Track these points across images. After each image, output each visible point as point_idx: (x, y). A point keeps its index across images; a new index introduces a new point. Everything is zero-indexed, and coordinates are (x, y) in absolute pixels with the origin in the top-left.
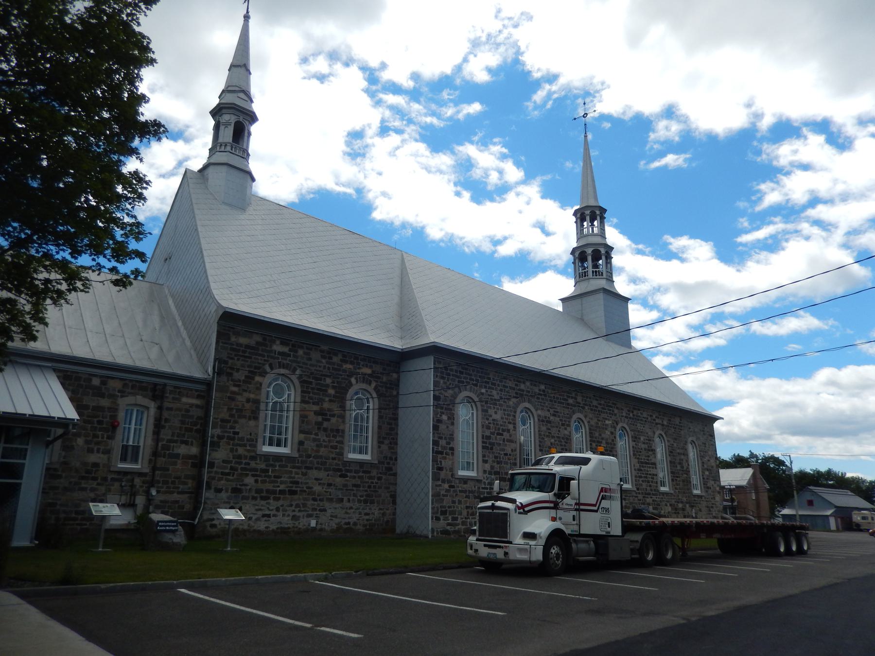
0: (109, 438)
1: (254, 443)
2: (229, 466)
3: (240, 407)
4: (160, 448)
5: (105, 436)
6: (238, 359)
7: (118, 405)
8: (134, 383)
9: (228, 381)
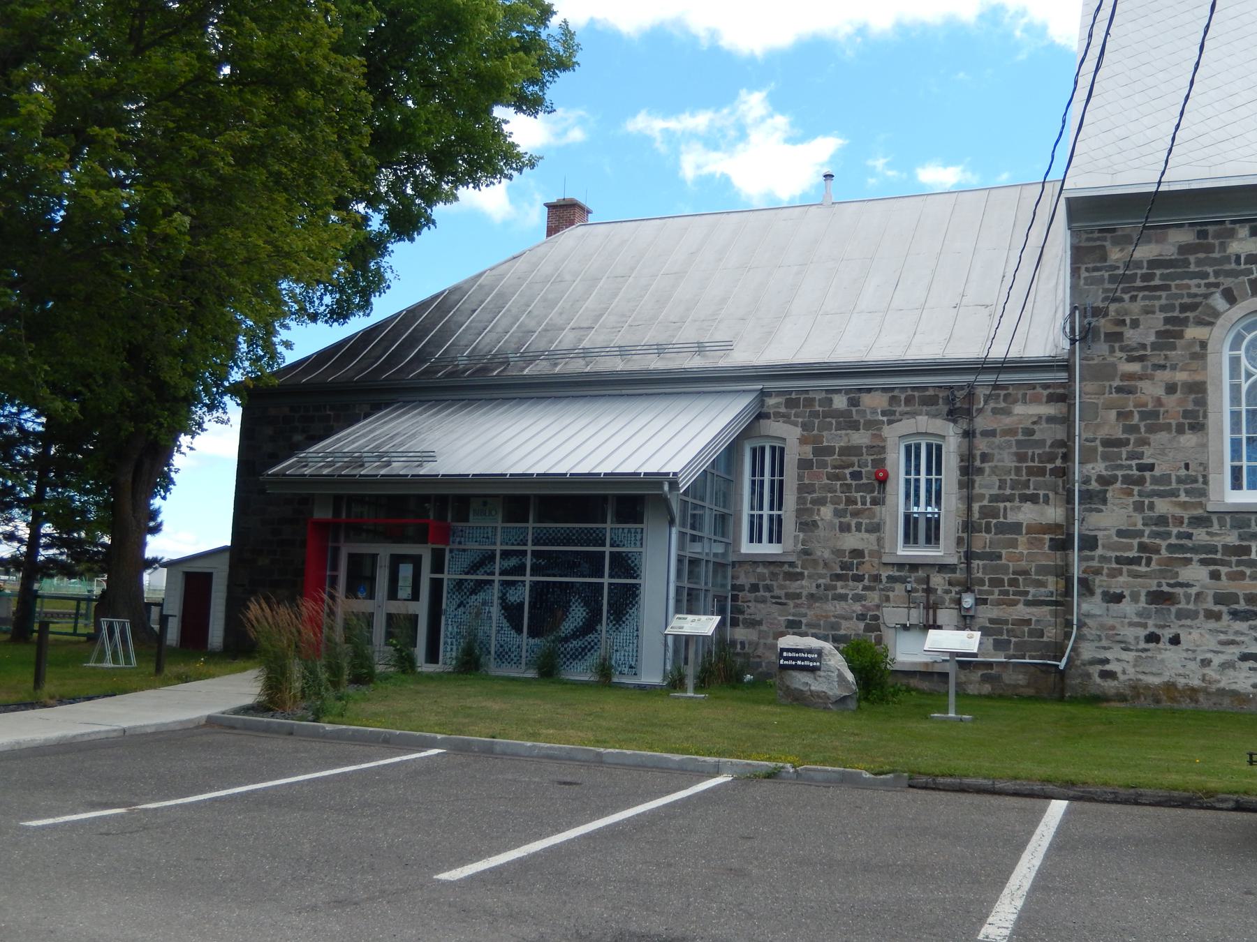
0: (875, 502)
1: (1199, 485)
2: (1135, 542)
3: (1150, 407)
4: (976, 515)
5: (868, 500)
6: (1133, 299)
7: (884, 440)
8: (910, 392)
9: (1112, 350)
